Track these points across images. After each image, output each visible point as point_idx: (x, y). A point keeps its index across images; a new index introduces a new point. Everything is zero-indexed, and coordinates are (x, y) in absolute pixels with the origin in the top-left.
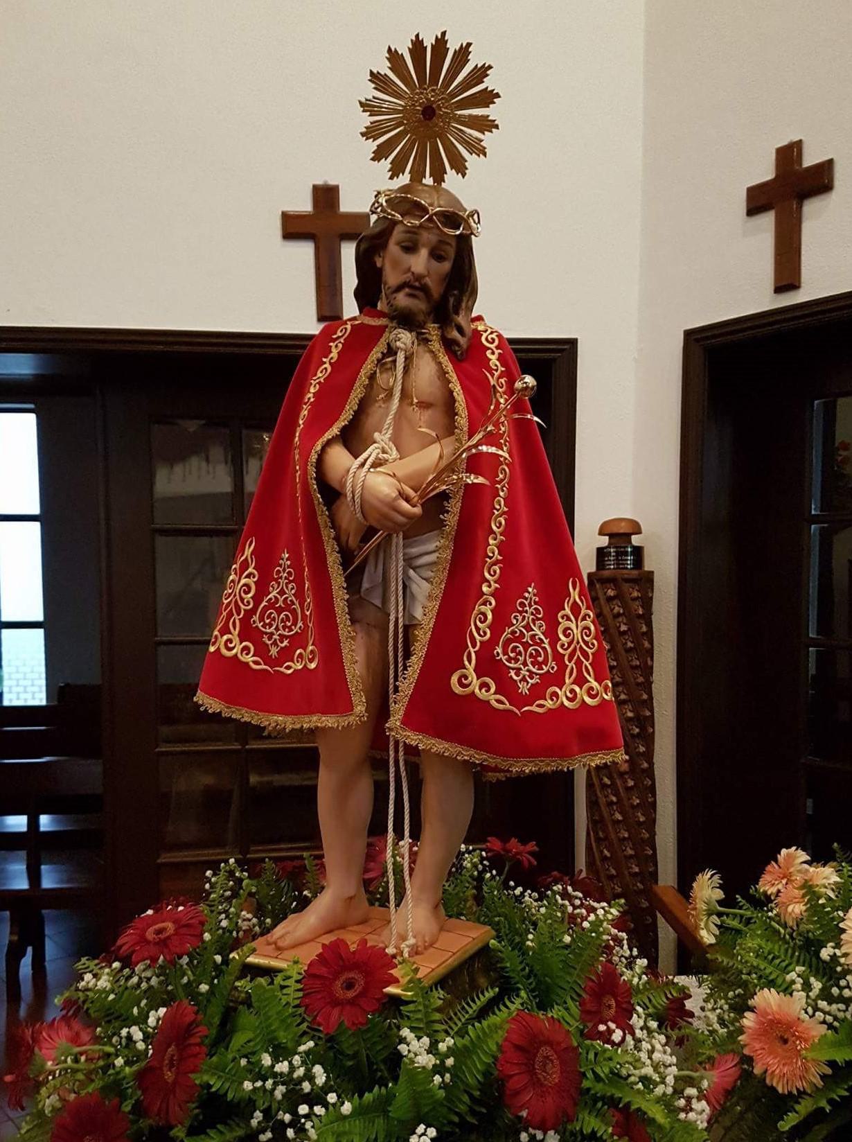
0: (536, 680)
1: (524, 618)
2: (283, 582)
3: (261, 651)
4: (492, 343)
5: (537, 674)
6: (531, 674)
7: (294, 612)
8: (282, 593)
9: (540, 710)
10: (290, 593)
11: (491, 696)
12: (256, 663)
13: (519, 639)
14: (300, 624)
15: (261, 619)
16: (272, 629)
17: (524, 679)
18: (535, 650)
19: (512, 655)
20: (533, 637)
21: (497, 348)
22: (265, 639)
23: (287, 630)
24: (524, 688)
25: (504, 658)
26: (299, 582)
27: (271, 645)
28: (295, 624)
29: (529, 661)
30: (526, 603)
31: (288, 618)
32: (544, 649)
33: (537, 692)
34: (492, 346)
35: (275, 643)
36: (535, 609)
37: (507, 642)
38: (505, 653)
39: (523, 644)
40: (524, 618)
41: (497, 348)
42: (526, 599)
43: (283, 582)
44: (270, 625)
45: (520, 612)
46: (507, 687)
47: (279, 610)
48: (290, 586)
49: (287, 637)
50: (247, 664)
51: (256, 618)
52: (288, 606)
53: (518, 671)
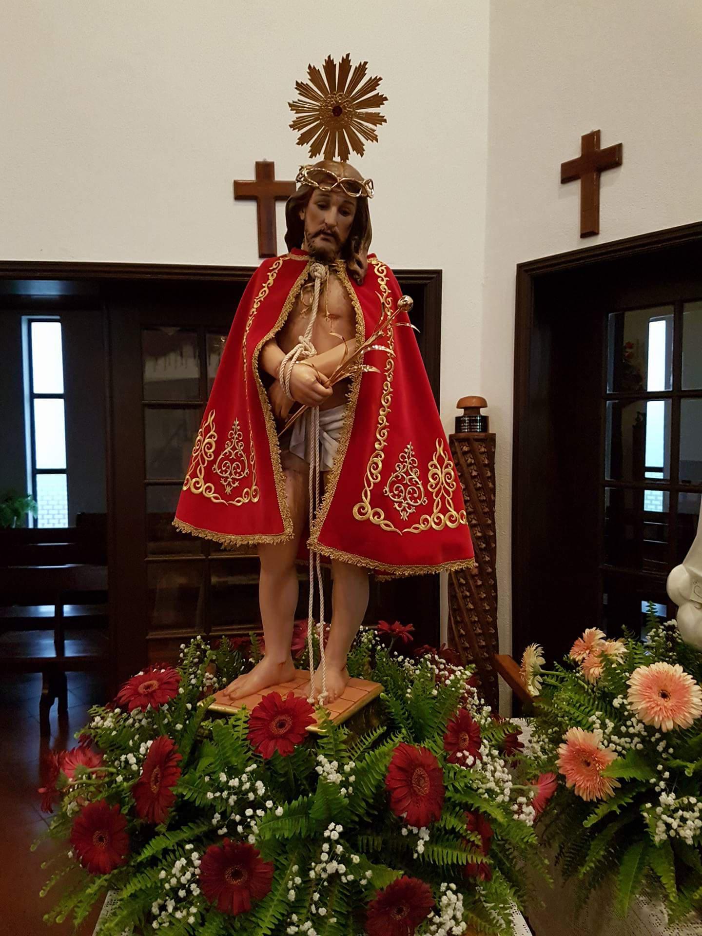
0: (413, 510)
1: (404, 466)
2: (235, 441)
4: (382, 273)
6: (410, 506)
7: (242, 462)
8: (234, 449)
9: (416, 531)
10: (240, 449)
11: (381, 521)
12: (216, 498)
14: (247, 471)
15: (220, 467)
17: (404, 509)
18: (412, 489)
19: (396, 492)
20: (411, 480)
21: (386, 276)
22: (222, 481)
23: (237, 475)
24: (404, 516)
26: (246, 441)
27: (227, 485)
28: (243, 470)
30: (406, 456)
31: (238, 467)
32: (418, 488)
33: (414, 519)
34: (382, 275)
36: (412, 460)
38: (391, 491)
39: (403, 484)
40: (404, 466)
41: (386, 276)
43: (235, 441)
45: (402, 463)
46: (392, 515)
47: (232, 461)
48: (240, 444)
49: (237, 480)
51: (216, 466)
53: (400, 504)
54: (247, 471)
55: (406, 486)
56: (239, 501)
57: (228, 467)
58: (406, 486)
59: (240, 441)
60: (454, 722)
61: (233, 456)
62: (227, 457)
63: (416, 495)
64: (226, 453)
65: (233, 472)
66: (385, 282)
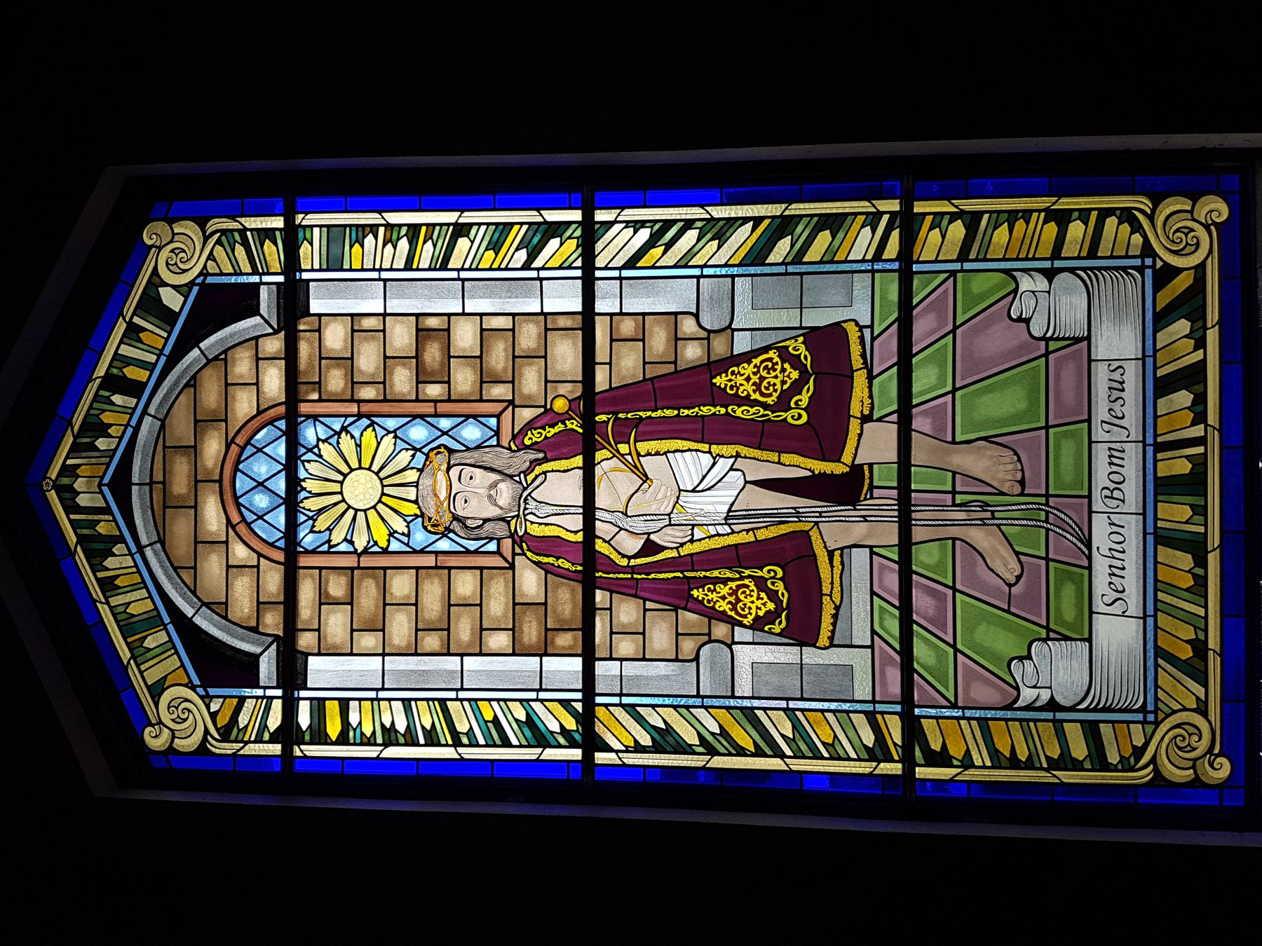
0: (787, 366)
1: (741, 385)
2: (714, 596)
3: (797, 387)
4: (542, 434)
5: (782, 366)
6: (783, 370)
7: (739, 587)
8: (724, 598)
9: (809, 358)
10: (725, 590)
11: (804, 398)
12: (780, 623)
13: (758, 386)
14: (746, 582)
15: (745, 617)
16: (753, 606)
17: (764, 604)
18: (763, 370)
19: (771, 388)
20: (755, 374)
21: (545, 430)
22: (761, 613)
23: (776, 367)
24: (771, 606)
25: (775, 395)
26: (716, 581)
27: (791, 379)
28: (747, 586)
29: (773, 374)
30: (729, 384)
31: (744, 592)
32: (762, 362)
33: (795, 362)
34: (544, 433)
35: (764, 604)
36: (732, 375)
37: (762, 394)
38: (771, 395)
39: (761, 382)
40: (741, 385)
41: (545, 430)
42: (726, 385)
43: (714, 596)
44: (750, 608)
45: (738, 389)
46: (797, 387)
47: (738, 600)
48: (718, 590)
49: (759, 595)
50: (810, 398)
51: (770, 401)
52: (734, 592)
53: (758, 608)
54: (746, 582)
55: (762, 379)
56: (806, 357)
57: (745, 605)
58: (762, 379)
59: (715, 590)
60: (1116, 706)
61: (732, 599)
62: (734, 608)
63: (770, 365)
64: (730, 609)
65: (773, 374)
66: (551, 429)
